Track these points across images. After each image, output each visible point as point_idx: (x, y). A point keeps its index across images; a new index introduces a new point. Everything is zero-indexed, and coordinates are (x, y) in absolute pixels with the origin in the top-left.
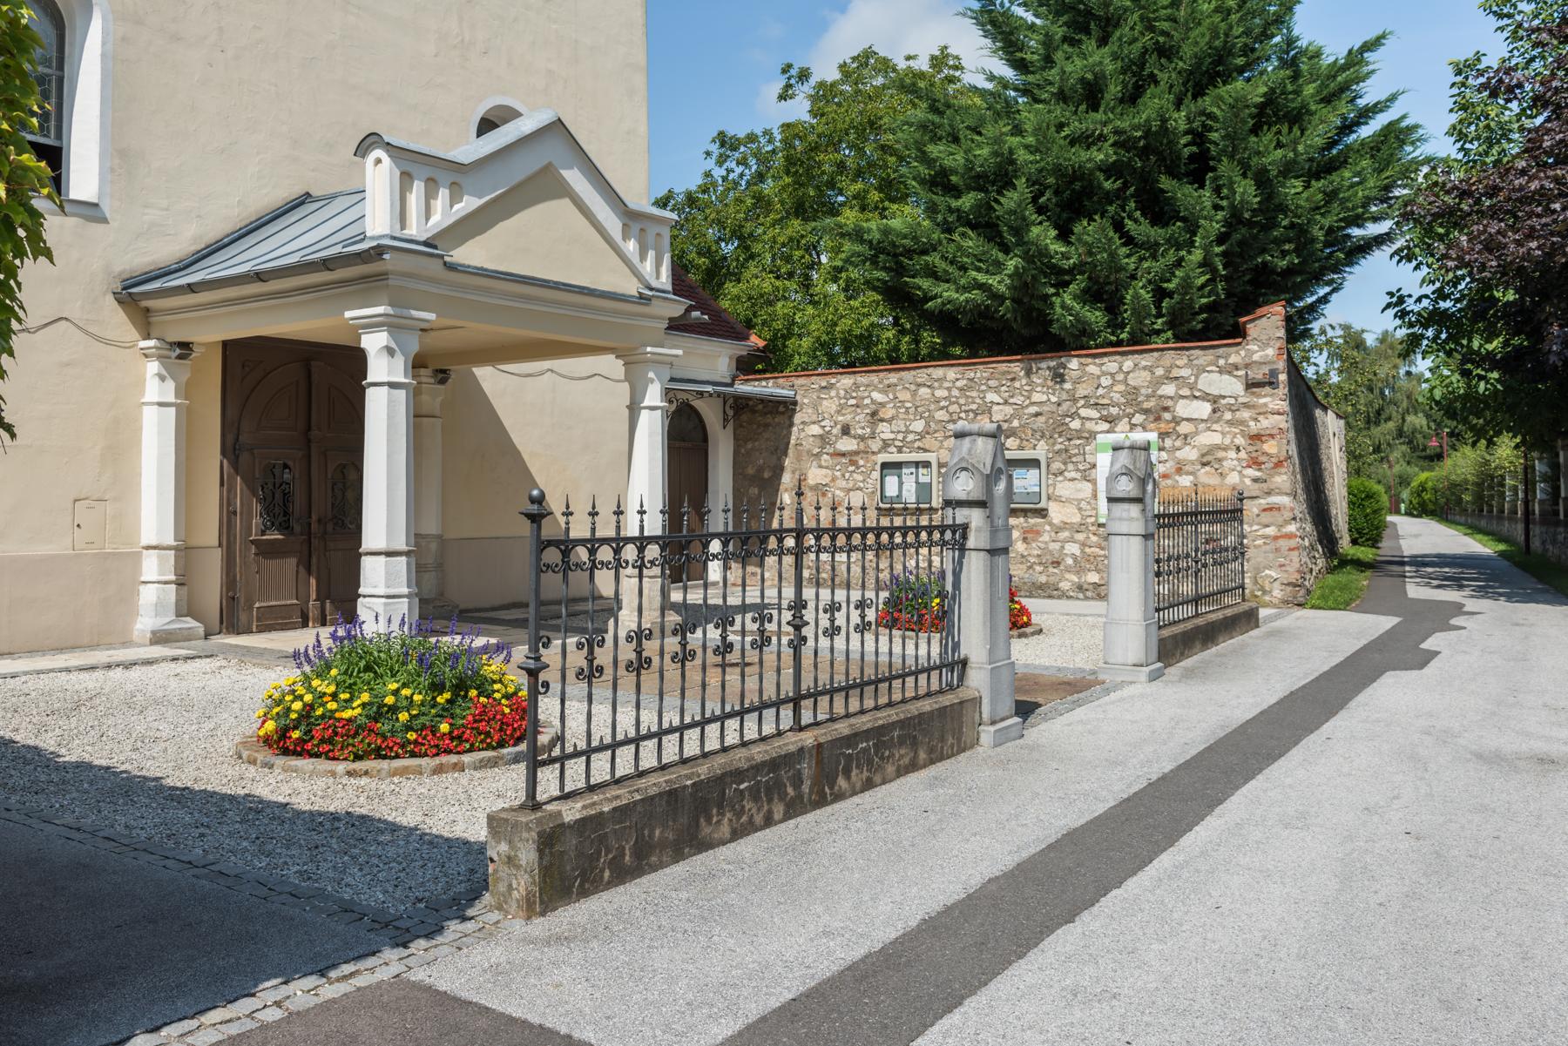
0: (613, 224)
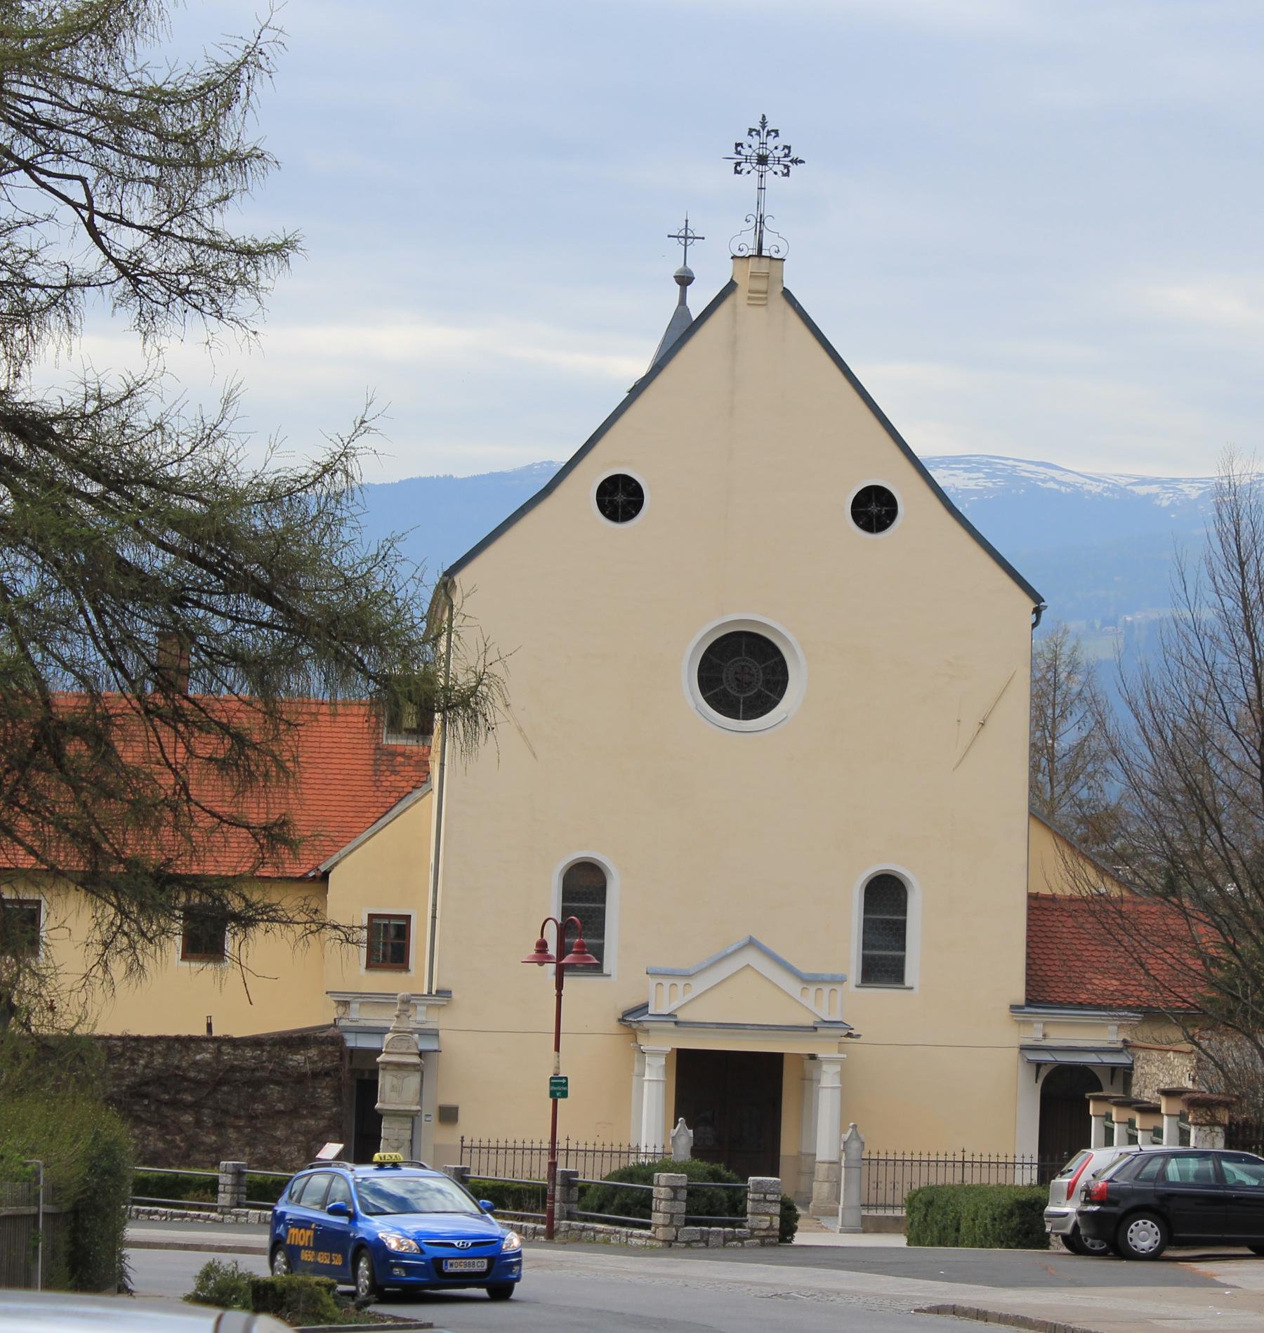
0: (792, 986)
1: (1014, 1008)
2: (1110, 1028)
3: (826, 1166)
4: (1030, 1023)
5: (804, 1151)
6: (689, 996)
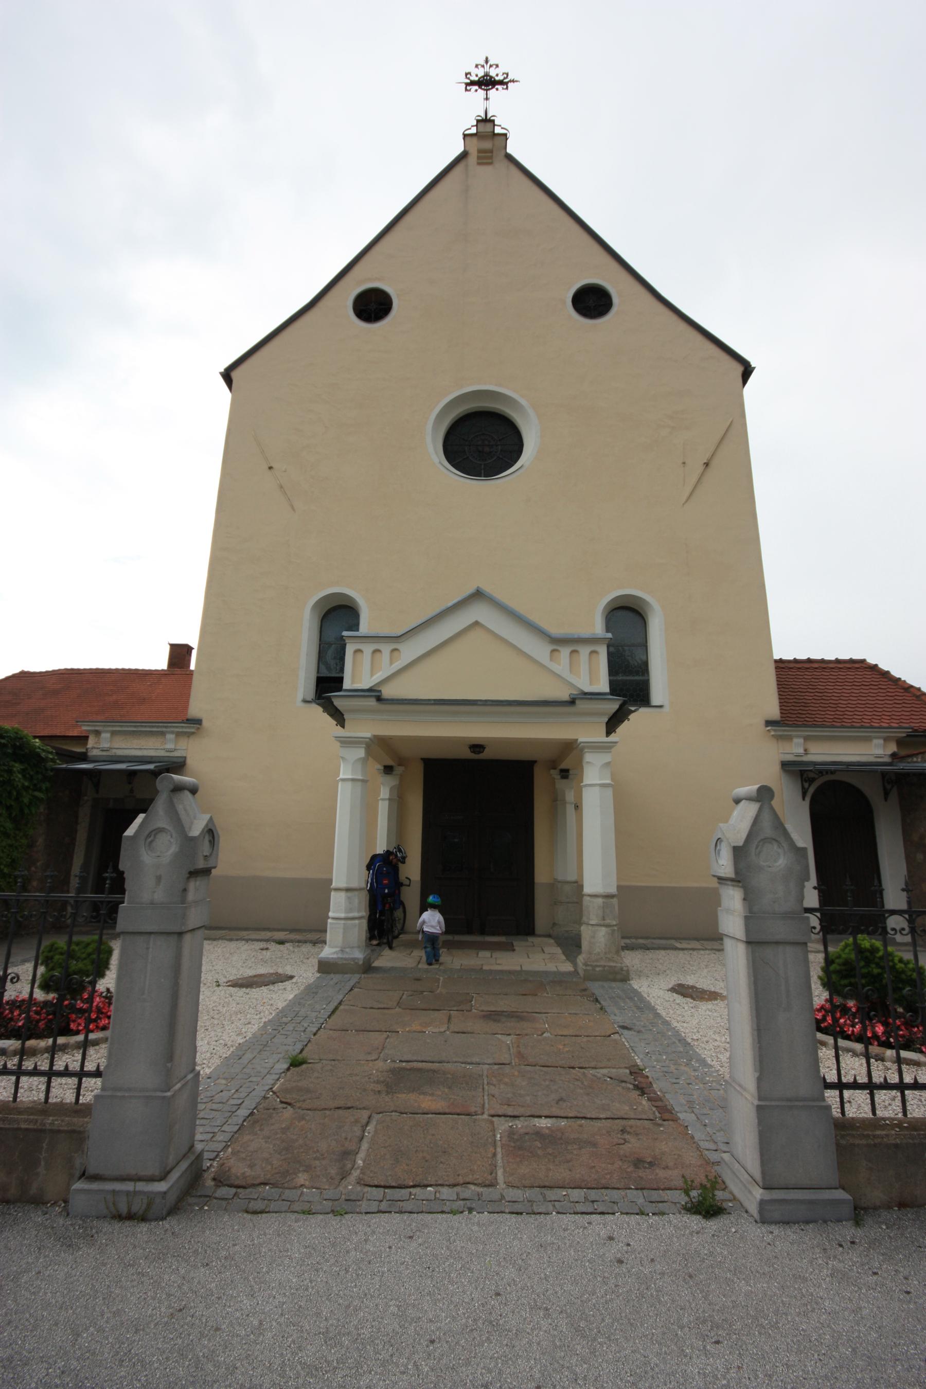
0: (540, 650)
1: (769, 723)
2: (875, 741)
3: (600, 901)
4: (789, 738)
5: (560, 878)
6: (397, 665)
